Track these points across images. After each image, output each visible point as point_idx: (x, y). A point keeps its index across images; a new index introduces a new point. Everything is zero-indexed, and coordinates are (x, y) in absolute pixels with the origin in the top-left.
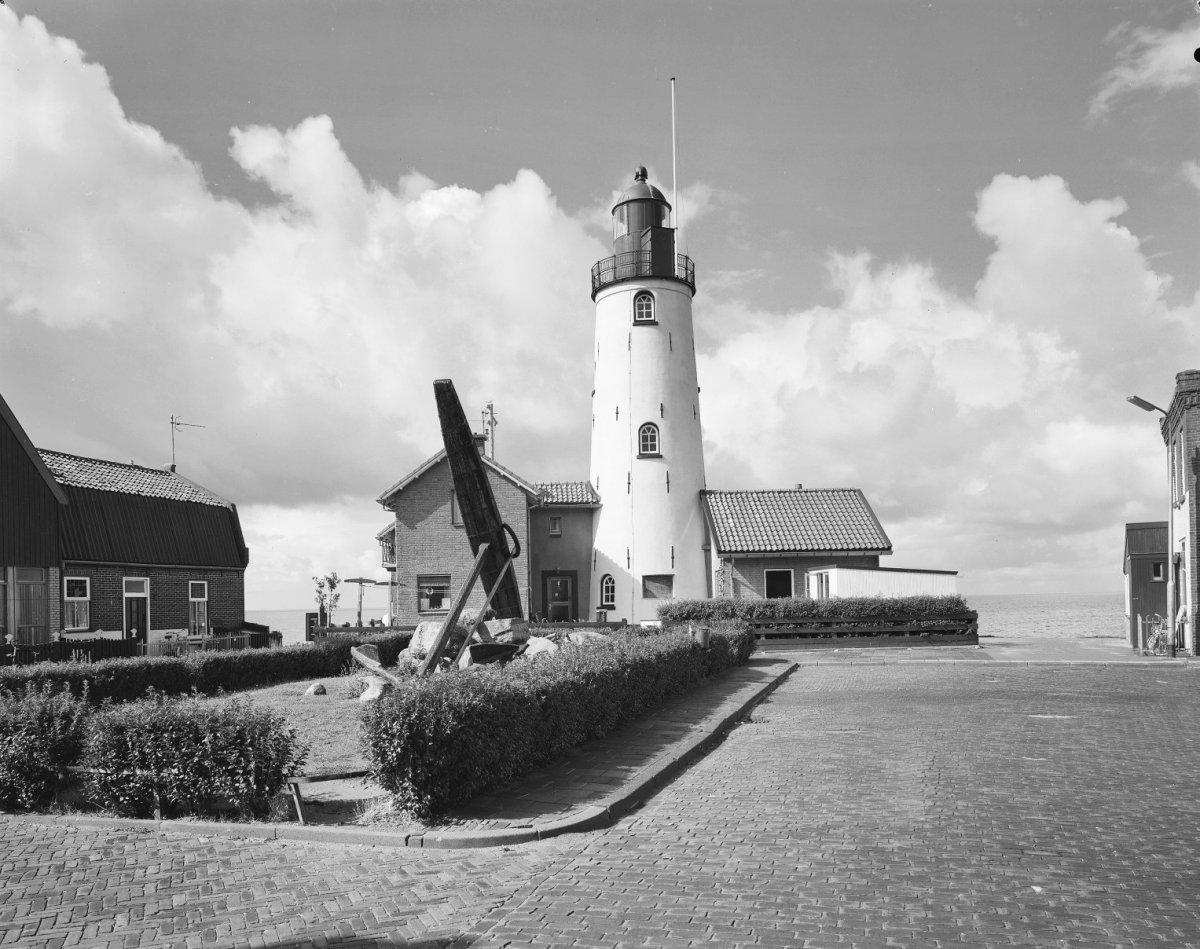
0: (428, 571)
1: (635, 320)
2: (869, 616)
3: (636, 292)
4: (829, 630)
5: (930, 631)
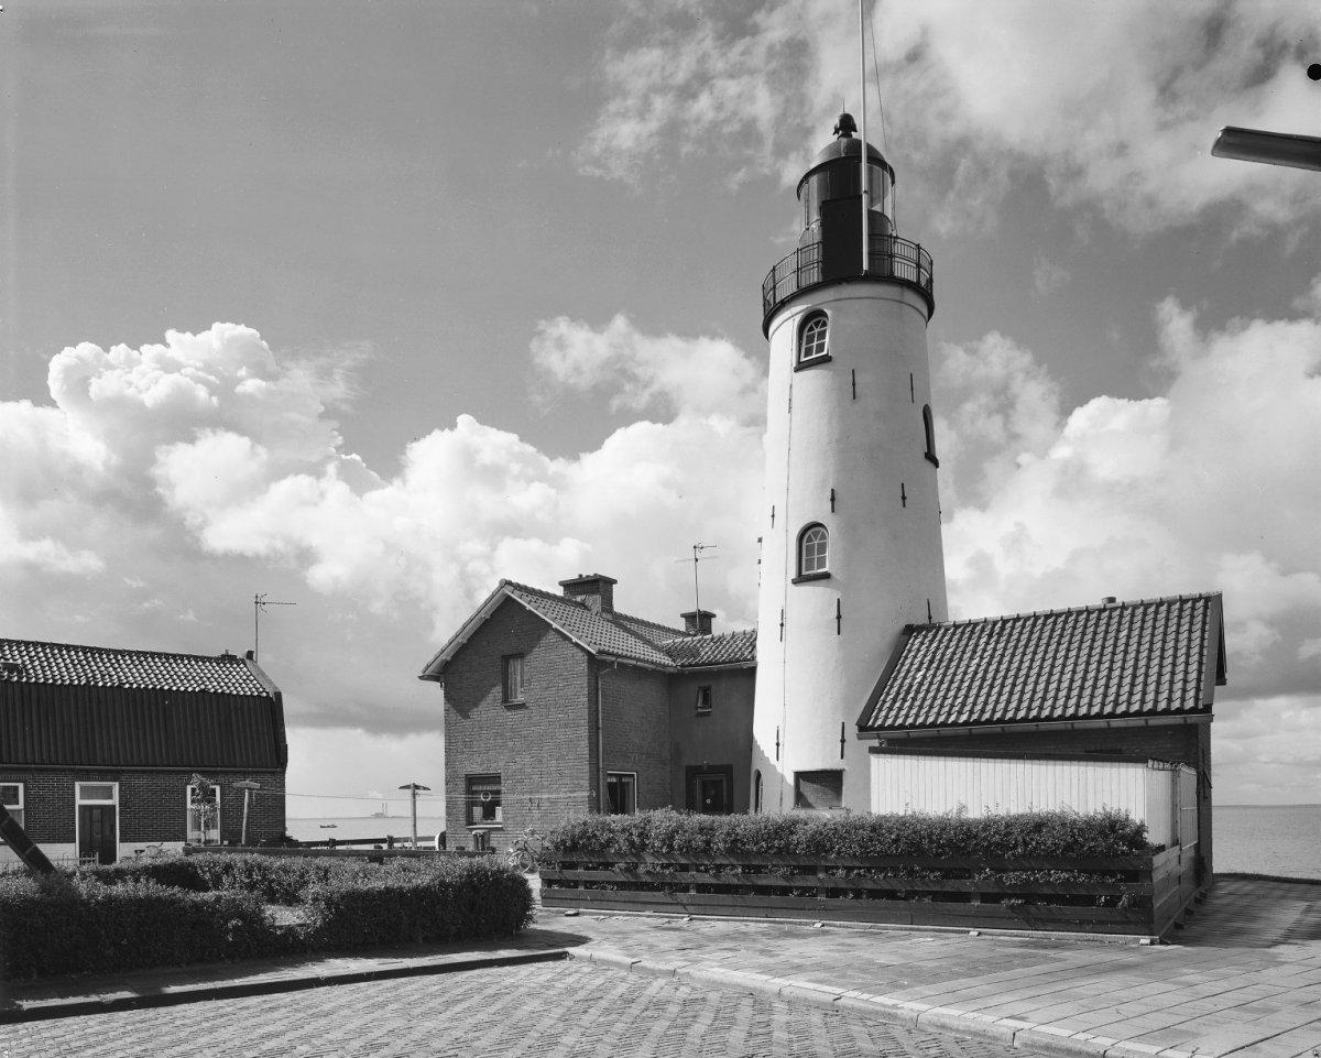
0: (477, 770)
1: (799, 362)
2: (884, 855)
3: (798, 319)
4: (811, 881)
5: (1029, 895)
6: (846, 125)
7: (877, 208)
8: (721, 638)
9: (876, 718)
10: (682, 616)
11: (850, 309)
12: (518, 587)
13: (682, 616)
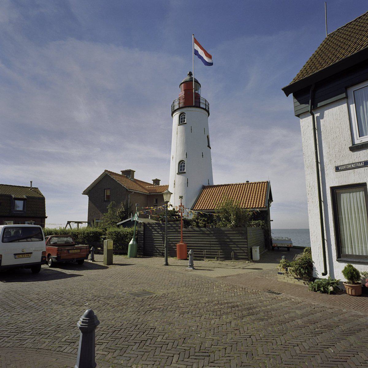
3: (179, 114)
6: (190, 74)
7: (197, 92)
8: (161, 186)
9: (196, 208)
10: (121, 171)
11: (190, 112)
12: (109, 172)
13: (121, 171)
